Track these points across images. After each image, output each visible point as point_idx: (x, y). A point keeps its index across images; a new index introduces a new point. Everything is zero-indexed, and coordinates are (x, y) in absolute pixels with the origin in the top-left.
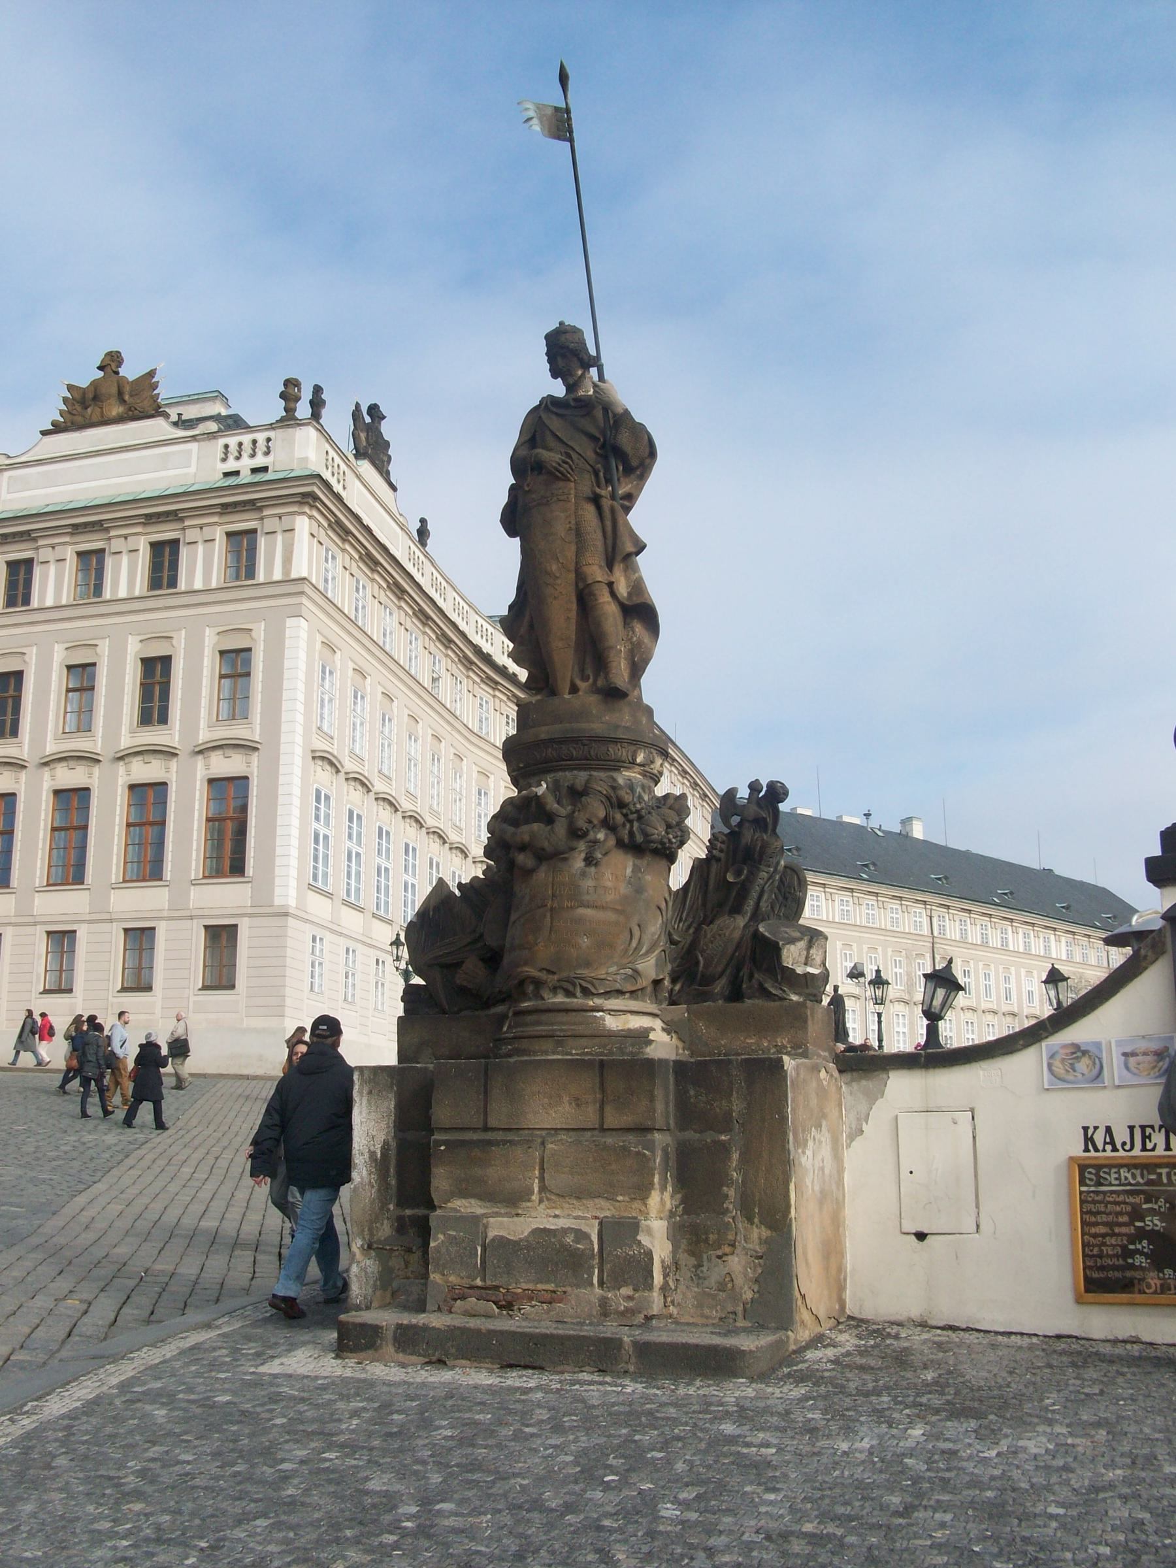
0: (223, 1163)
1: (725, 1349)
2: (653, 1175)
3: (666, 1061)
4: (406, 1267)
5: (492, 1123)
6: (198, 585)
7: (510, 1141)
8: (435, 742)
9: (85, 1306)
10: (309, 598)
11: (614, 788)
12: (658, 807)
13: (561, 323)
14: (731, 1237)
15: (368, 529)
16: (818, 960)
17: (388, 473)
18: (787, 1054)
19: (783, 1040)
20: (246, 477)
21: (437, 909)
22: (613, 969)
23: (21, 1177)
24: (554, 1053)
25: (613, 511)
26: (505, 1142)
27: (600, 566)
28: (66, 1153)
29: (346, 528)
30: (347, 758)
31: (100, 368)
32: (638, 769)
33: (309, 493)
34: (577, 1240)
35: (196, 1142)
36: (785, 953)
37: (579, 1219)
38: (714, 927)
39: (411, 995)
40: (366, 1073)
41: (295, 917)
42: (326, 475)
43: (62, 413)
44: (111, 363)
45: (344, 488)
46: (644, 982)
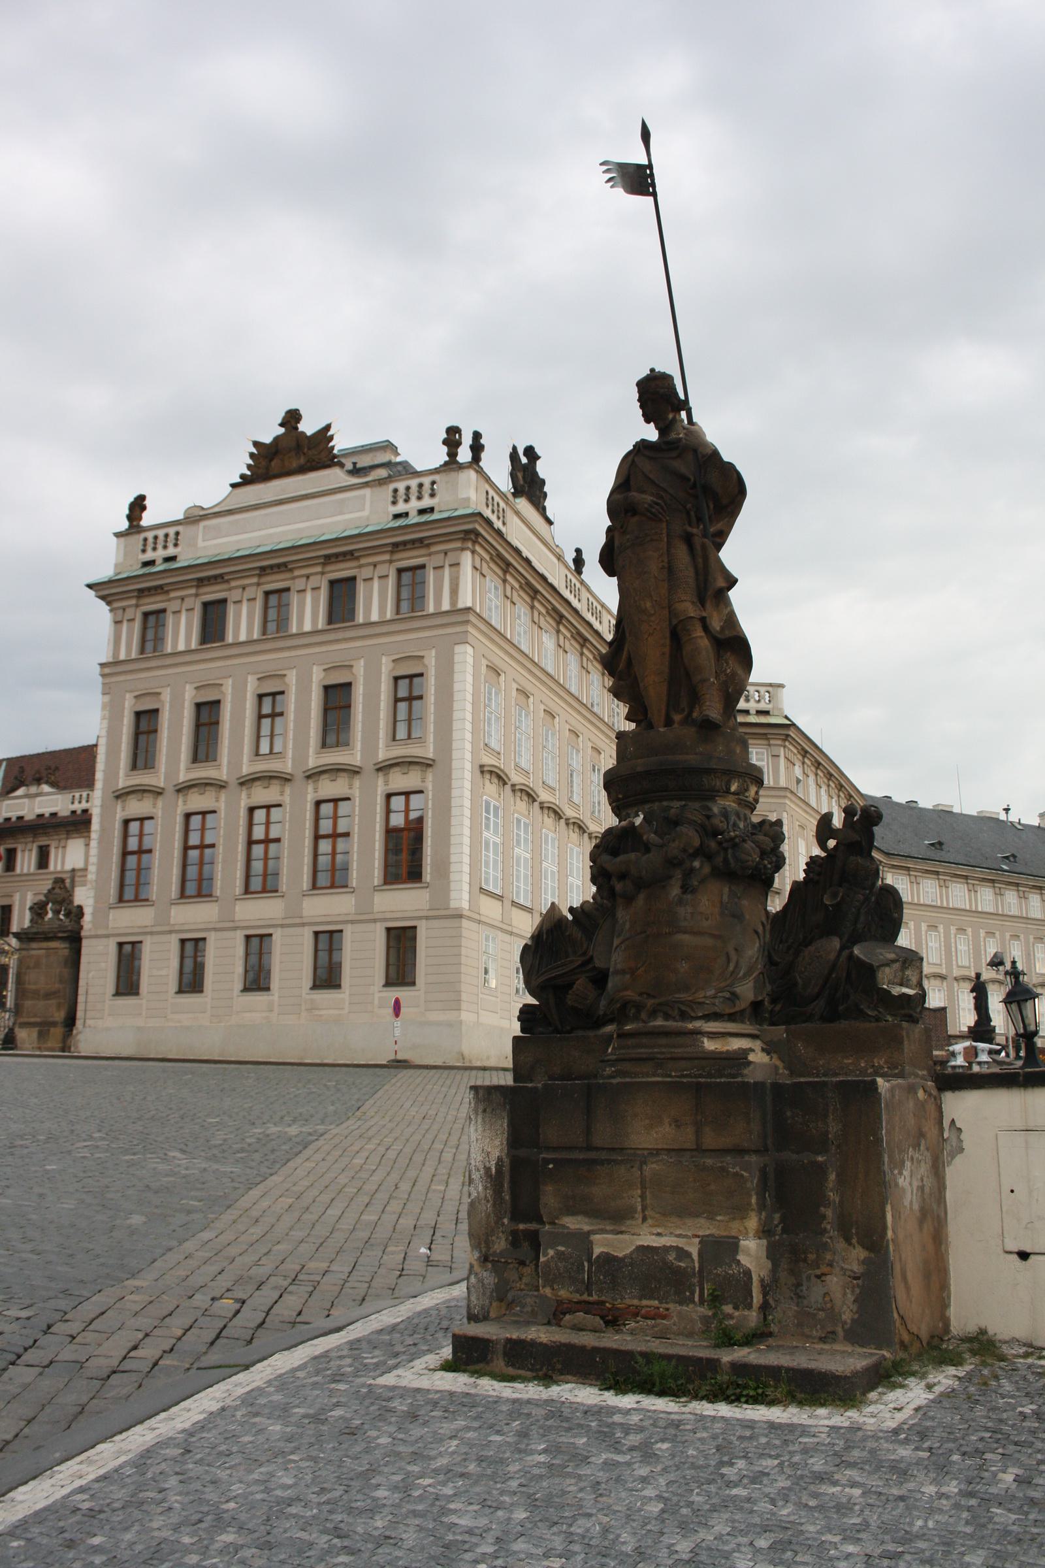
0: (391, 1154)
1: (820, 1373)
2: (751, 1196)
3: (763, 1084)
4: (520, 1279)
5: (597, 1141)
6: (375, 617)
7: (614, 1161)
8: (595, 754)
9: (238, 1306)
10: (475, 626)
11: (708, 817)
12: (753, 834)
13: (652, 370)
14: (828, 1257)
15: (527, 561)
16: (914, 980)
17: (544, 508)
18: (882, 1076)
19: (879, 1061)
20: (414, 519)
21: (550, 931)
22: (711, 992)
23: (205, 1169)
24: (654, 1076)
25: (704, 547)
26: (609, 1161)
27: (693, 603)
28: (250, 1145)
29: (508, 563)
30: (513, 772)
31: (281, 425)
32: (732, 797)
33: (472, 531)
34: (679, 1258)
35: (370, 1133)
36: (880, 975)
37: (676, 1237)
38: (811, 948)
39: (526, 1015)
40: (481, 1092)
41: (469, 918)
42: (487, 513)
43: (249, 467)
44: (292, 418)
45: (504, 524)
46: (742, 1005)
